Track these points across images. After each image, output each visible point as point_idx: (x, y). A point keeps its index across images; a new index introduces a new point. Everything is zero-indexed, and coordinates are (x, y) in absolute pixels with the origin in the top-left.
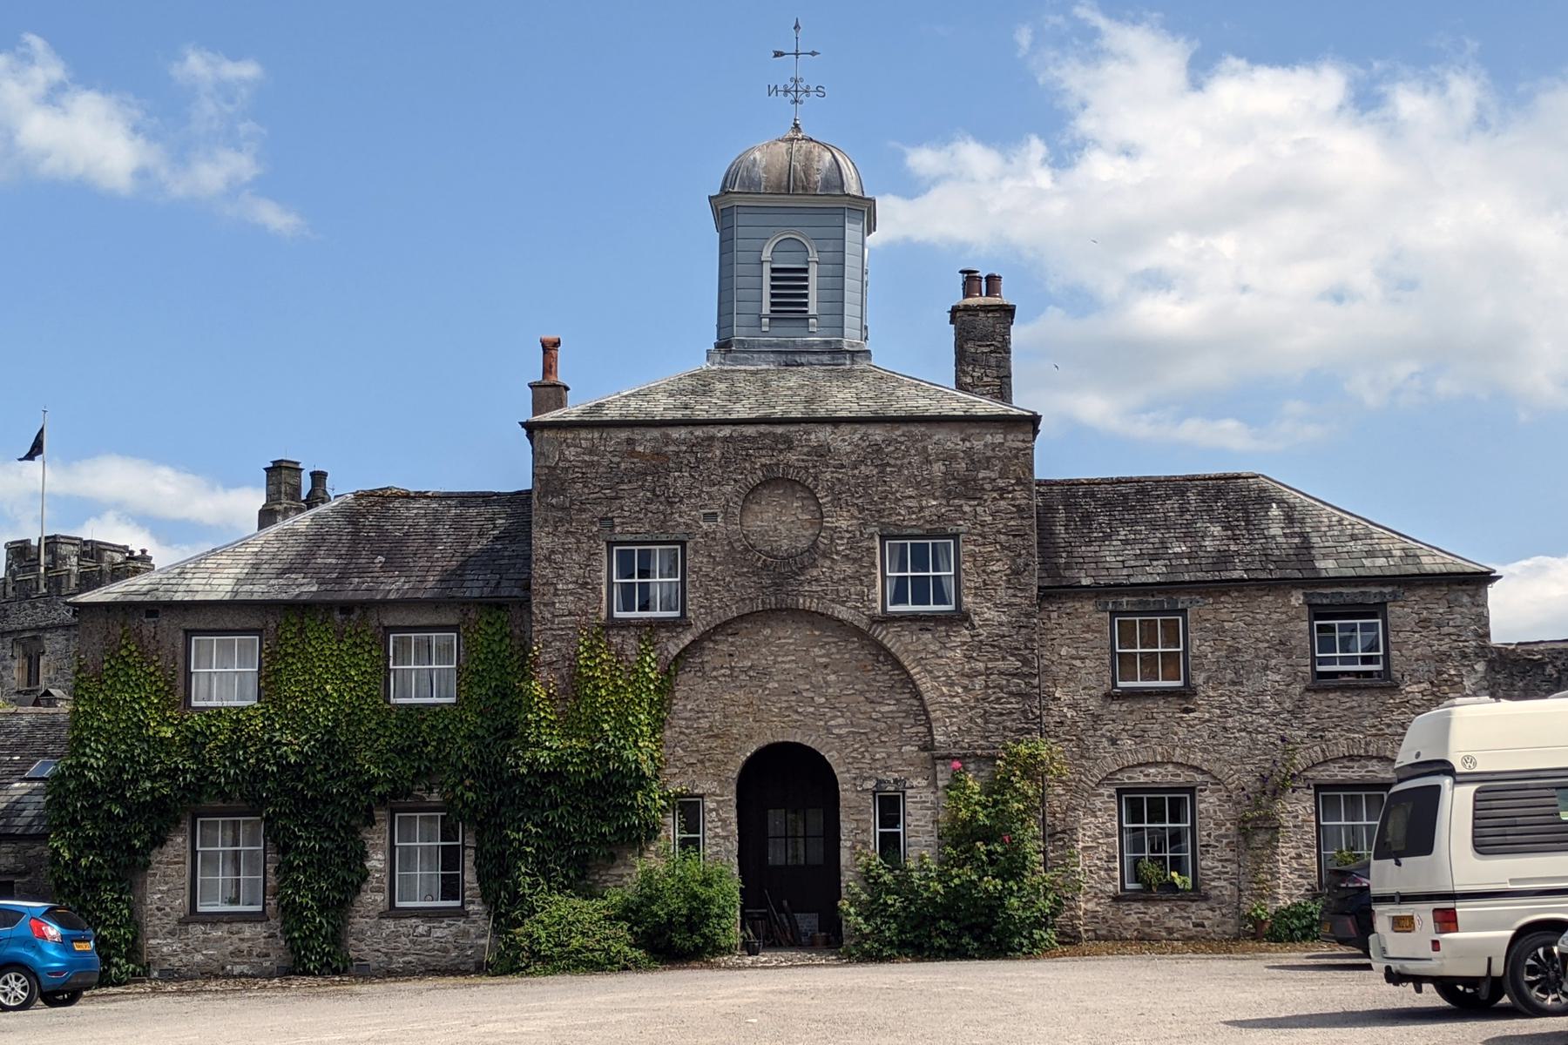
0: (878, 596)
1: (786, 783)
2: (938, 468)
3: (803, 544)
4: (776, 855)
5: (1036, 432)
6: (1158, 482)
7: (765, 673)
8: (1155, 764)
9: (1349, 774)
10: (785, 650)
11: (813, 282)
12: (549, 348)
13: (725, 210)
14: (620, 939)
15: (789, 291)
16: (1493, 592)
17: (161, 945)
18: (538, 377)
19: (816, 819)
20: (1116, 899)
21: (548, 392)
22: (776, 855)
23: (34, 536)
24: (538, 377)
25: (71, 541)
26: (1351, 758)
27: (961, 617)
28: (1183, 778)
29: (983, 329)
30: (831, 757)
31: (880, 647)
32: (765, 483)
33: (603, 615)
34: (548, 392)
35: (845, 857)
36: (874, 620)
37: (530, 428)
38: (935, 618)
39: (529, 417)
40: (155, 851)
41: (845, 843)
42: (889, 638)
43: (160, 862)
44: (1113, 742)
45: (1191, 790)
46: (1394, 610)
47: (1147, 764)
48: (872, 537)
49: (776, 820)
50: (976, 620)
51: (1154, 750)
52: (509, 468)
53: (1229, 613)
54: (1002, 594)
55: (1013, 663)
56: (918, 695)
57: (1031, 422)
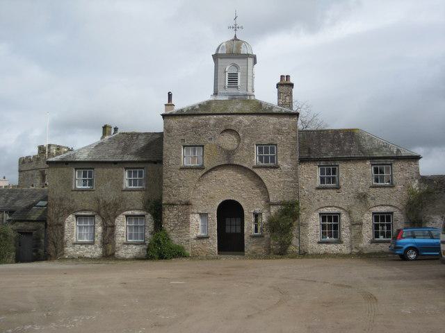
0: (256, 160)
1: (230, 211)
2: (271, 127)
3: (235, 147)
4: (228, 230)
5: (298, 117)
6: (340, 130)
7: (225, 181)
8: (330, 207)
9: (381, 210)
10: (228, 175)
11: (239, 77)
12: (170, 95)
13: (216, 57)
14: (157, 256)
15: (233, 79)
16: (420, 161)
17: (239, 230)
18: (167, 103)
19: (238, 222)
20: (319, 243)
21: (170, 104)
22: (228, 230)
23: (45, 144)
24: (167, 103)
25: (54, 145)
26: (382, 205)
27: (276, 167)
28: (337, 210)
29: (285, 85)
30: (242, 204)
31: (256, 174)
32: (225, 131)
33: (74, 187)
34: (170, 104)
35: (245, 230)
36: (254, 167)
37: (164, 116)
38: (271, 167)
39: (164, 112)
40: (116, 220)
41: (246, 227)
42: (256, 171)
43: (193, 213)
44: (319, 200)
45: (339, 214)
46: (394, 165)
47: (327, 207)
48: (253, 145)
49: (228, 221)
50: (281, 167)
51: (332, 202)
52: (158, 126)
53: (351, 167)
54: (289, 160)
55: (291, 179)
56: (266, 188)
57: (297, 114)
